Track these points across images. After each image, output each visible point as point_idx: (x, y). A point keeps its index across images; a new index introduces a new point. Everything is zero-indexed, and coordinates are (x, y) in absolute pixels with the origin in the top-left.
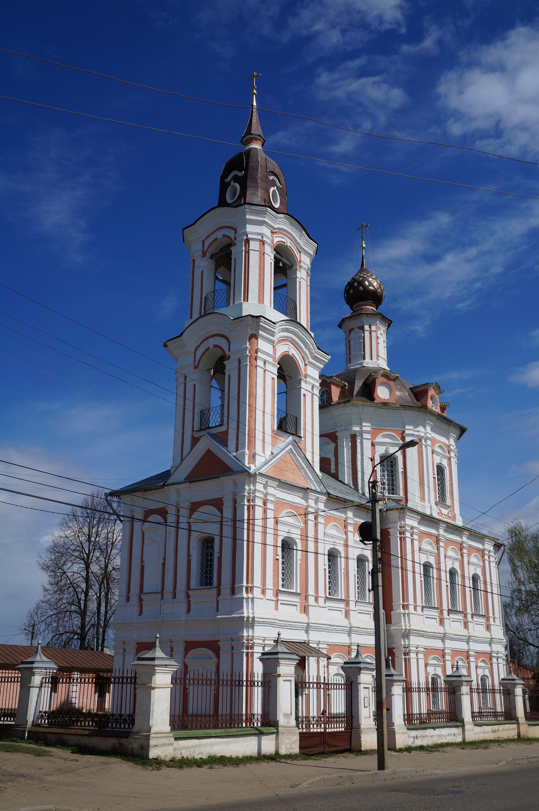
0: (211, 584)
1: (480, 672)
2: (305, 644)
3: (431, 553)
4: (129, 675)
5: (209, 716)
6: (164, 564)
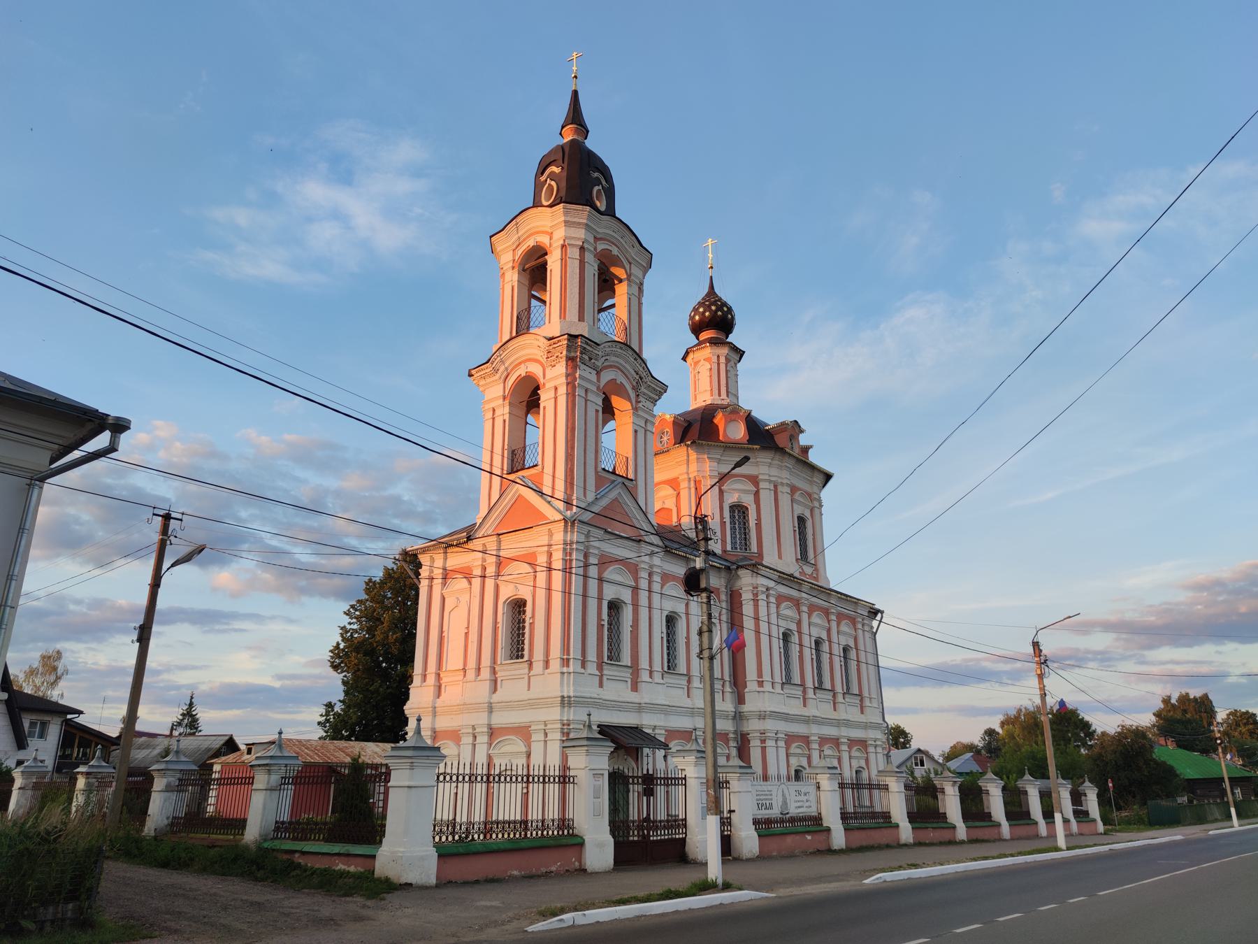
0: (522, 657)
1: (855, 764)
2: (636, 730)
3: (850, 635)
4: (520, 772)
5: (515, 822)
6: (467, 634)
